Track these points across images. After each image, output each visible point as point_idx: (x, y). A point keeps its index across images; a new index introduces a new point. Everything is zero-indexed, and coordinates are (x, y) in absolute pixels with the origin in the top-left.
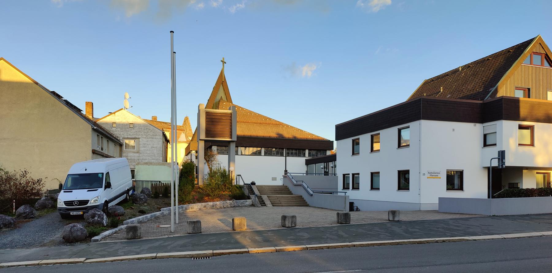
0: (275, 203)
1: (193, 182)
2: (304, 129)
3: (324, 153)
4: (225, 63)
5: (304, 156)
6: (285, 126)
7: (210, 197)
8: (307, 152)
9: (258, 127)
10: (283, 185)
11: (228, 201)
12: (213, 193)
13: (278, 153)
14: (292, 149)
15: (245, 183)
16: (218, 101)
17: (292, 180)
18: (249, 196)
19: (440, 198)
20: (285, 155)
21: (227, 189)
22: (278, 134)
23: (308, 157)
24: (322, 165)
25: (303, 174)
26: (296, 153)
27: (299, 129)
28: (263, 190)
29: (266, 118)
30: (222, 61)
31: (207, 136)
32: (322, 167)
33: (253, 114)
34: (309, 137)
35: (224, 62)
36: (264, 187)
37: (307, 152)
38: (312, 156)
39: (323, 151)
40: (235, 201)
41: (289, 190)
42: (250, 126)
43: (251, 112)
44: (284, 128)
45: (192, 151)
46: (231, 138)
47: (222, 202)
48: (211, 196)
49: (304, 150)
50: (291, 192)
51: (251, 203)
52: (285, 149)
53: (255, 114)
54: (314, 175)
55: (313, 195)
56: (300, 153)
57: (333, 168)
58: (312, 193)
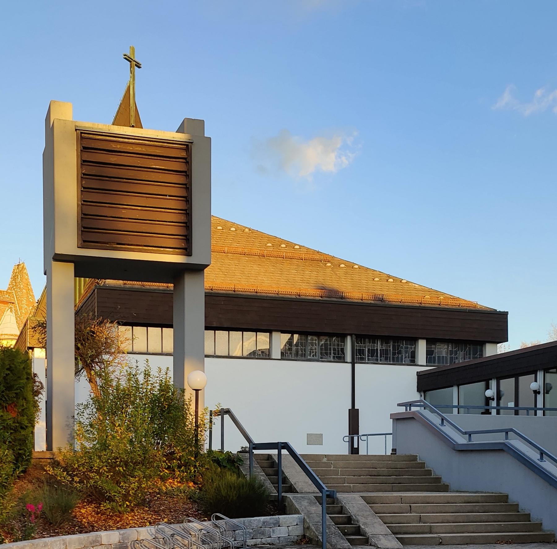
0: (405, 530)
1: (23, 432)
2: (405, 279)
3: (475, 354)
5: (413, 361)
6: (342, 266)
7: (106, 506)
8: (422, 347)
9: (255, 267)
11: (195, 525)
12: (118, 483)
13: (326, 349)
14: (373, 338)
15: (256, 441)
17: (442, 428)
18: (284, 498)
20: (349, 358)
21: (179, 467)
22: (323, 288)
23: (425, 364)
26: (387, 350)
27: (389, 276)
29: (277, 242)
30: (128, 59)
31: (84, 243)
33: (233, 229)
34: (428, 300)
36: (325, 460)
37: (422, 347)
38: (439, 362)
39: (472, 347)
40: (225, 522)
41: (429, 472)
42: (227, 261)
45: (32, 348)
46: (187, 251)
47: (167, 529)
48: (111, 499)
49: (414, 340)
51: (297, 532)
52: (349, 339)
53: (241, 229)
54: (455, 410)
56: (400, 352)
57: (540, 398)
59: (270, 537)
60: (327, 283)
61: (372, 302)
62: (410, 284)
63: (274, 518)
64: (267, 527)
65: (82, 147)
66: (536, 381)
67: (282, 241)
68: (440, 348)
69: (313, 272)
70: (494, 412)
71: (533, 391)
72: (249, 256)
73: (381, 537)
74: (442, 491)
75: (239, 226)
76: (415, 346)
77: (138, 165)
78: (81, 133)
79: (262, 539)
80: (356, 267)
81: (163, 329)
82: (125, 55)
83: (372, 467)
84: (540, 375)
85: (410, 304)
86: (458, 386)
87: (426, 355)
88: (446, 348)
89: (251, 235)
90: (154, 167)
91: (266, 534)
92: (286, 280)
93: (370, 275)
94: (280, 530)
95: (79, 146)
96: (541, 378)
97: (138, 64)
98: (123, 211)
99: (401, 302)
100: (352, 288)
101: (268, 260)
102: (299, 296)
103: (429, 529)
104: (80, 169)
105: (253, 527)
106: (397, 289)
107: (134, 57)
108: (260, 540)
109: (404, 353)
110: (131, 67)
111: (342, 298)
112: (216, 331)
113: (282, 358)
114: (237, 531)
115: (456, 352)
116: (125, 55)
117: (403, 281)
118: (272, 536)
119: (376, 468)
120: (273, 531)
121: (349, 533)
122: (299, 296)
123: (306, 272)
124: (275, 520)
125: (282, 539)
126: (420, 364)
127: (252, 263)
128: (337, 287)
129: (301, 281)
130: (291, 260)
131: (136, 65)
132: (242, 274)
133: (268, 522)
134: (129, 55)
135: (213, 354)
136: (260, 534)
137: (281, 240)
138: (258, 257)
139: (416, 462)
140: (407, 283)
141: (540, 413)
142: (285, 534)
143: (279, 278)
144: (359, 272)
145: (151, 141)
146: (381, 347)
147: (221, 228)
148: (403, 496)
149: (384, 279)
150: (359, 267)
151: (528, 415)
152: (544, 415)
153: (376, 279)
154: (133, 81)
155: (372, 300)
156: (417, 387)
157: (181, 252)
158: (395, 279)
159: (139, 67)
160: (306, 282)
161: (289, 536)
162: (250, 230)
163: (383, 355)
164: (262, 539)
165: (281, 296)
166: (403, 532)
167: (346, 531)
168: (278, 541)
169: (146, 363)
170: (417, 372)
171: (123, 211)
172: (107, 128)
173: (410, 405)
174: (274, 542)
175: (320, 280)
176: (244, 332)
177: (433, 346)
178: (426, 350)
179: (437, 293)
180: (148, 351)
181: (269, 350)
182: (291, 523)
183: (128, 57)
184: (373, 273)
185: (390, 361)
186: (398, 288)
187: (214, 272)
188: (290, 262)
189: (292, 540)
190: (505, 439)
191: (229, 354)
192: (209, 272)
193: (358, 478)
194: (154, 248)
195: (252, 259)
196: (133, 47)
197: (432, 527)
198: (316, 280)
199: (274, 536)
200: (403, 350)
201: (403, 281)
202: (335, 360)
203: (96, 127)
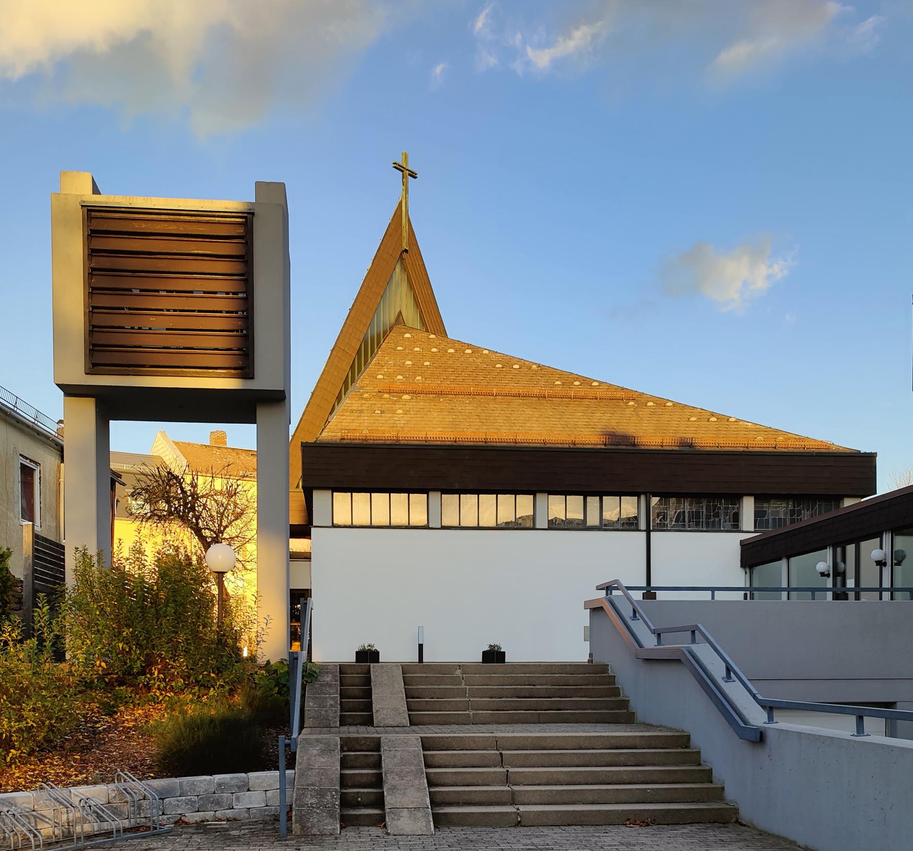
2: (734, 415)
4: (413, 175)
5: (735, 525)
6: (650, 404)
8: (748, 506)
10: (590, 661)
14: (680, 496)
16: (378, 336)
19: (504, 652)
23: (753, 530)
24: (823, 561)
25: (713, 590)
26: (698, 513)
27: (713, 414)
28: (445, 693)
29: (568, 378)
30: (398, 167)
31: (94, 367)
32: (822, 566)
34: (760, 443)
35: (409, 173)
37: (748, 506)
41: (616, 692)
42: (492, 406)
43: (508, 361)
44: (644, 413)
46: (245, 370)
49: (736, 498)
50: (625, 704)
53: (525, 365)
54: (784, 594)
55: (771, 738)
56: (717, 515)
57: (887, 571)
58: (757, 717)
59: (233, 808)
60: (620, 427)
61: (677, 448)
62: (741, 423)
63: (238, 778)
64: (225, 792)
65: (90, 230)
66: (881, 548)
67: (578, 378)
68: (776, 507)
69: (606, 415)
70: (852, 595)
71: (876, 562)
72: (525, 398)
73: (405, 813)
74: (623, 721)
75: (527, 363)
76: (739, 505)
77: (172, 252)
78: (88, 210)
79: (215, 811)
80: (670, 404)
81: (391, 494)
82: (394, 164)
83: (527, 683)
84: (887, 538)
85: (731, 449)
86: (788, 558)
87: (755, 517)
88: (784, 507)
89: (540, 372)
90: (196, 252)
91: (224, 804)
92: (565, 426)
93: (687, 413)
94: (250, 797)
95: (86, 230)
96: (887, 544)
97: (413, 173)
98: (151, 319)
99: (718, 447)
100: (654, 431)
101: (550, 402)
102: (574, 444)
103: (511, 798)
104: (87, 262)
105: (199, 792)
106: (719, 430)
107: (406, 164)
108: (213, 813)
109: (722, 515)
110: (403, 178)
111: (634, 445)
112: (461, 495)
113: (550, 527)
114: (167, 799)
115: (799, 511)
116: (394, 164)
117: (731, 420)
118: (235, 807)
119: (534, 685)
120: (238, 798)
121: (365, 803)
122: (574, 444)
123: (597, 415)
124: (241, 782)
125: (254, 811)
126: (744, 529)
127: (525, 407)
128: (634, 431)
129: (584, 426)
130: (580, 400)
131: (409, 175)
132: (506, 420)
133: (228, 783)
134: (401, 163)
135: (457, 525)
136: (212, 803)
137: (577, 376)
138: (537, 398)
139: (607, 674)
140: (736, 421)
141: (886, 595)
142: (259, 804)
143: (555, 423)
144: (673, 411)
145: (195, 216)
146: (689, 509)
147: (500, 366)
148: (499, 737)
149: (704, 418)
150: (673, 405)
151: (813, 599)
152: (892, 599)
153: (693, 419)
154: (406, 195)
155: (677, 446)
156: (741, 561)
157: (238, 373)
158: (720, 418)
159: (415, 178)
160: (592, 427)
161: (267, 806)
162: (539, 366)
163: (693, 519)
164: (215, 811)
165: (549, 445)
166: (464, 801)
167: (359, 799)
168: (247, 815)
169: (138, 535)
170: (741, 541)
171: (151, 319)
172: (128, 201)
173: (607, 587)
174: (240, 815)
175: (612, 424)
176: (499, 495)
177: (765, 505)
178: (755, 511)
179: (776, 433)
180: (371, 523)
181: (534, 517)
182: (270, 785)
183: (399, 165)
184: (692, 411)
185: (702, 528)
186: (721, 429)
187: (468, 420)
188: (579, 403)
189: (272, 813)
190: (690, 642)
191: (478, 524)
192: (462, 420)
193: (490, 701)
194: (198, 370)
195: (527, 401)
196: (406, 153)
197: (517, 793)
198: (606, 424)
199: (239, 807)
200: (722, 512)
201: (731, 420)
202: (625, 528)
203: (111, 201)
